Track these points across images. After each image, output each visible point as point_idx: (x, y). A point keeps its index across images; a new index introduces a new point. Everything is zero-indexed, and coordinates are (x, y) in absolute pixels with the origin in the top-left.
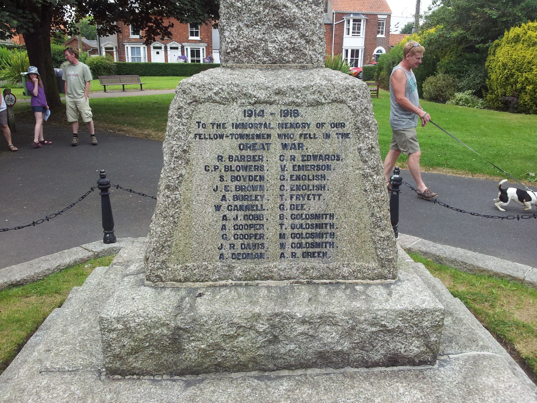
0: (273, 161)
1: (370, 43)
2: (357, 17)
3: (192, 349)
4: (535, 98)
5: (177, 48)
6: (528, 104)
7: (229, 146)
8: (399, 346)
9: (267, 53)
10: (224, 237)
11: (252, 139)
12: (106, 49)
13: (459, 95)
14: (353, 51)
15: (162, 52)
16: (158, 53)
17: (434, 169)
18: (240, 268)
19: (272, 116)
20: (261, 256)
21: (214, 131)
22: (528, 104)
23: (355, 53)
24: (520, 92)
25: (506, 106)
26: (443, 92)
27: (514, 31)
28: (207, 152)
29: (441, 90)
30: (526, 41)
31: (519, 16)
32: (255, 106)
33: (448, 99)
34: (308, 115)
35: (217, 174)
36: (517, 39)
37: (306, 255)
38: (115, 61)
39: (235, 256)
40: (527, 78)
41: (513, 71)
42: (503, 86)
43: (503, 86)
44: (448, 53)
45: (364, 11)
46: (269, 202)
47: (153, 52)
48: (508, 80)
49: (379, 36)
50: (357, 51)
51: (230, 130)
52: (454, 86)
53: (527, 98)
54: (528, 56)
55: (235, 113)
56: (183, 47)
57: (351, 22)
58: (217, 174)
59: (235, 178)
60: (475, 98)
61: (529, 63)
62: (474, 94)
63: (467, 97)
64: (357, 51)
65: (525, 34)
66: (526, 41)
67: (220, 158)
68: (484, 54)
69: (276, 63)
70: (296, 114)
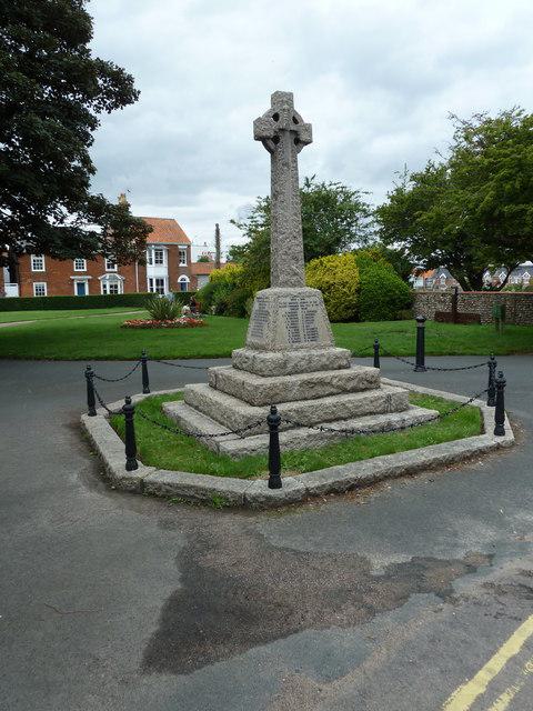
1: (174, 271)
3: (290, 367)
7: (288, 309)
11: (294, 307)
14: (157, 281)
19: (298, 300)
28: (282, 311)
34: (307, 299)
38: (87, 294)
46: (300, 325)
55: (288, 300)
57: (153, 252)
64: (162, 281)
69: (294, 285)
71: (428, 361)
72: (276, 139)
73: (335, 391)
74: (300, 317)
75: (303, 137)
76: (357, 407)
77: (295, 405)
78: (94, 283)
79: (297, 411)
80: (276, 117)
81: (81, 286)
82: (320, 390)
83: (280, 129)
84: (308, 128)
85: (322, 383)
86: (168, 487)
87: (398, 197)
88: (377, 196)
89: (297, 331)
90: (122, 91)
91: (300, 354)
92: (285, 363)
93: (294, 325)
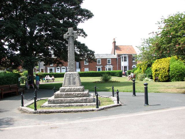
0: (71, 78)
2: (125, 56)
3: (66, 90)
5: (64, 68)
7: (68, 77)
8: (80, 90)
11: (70, 77)
12: (41, 69)
14: (125, 67)
15: (59, 70)
16: (58, 70)
23: (125, 67)
32: (70, 74)
45: (127, 54)
47: (57, 70)
49: (133, 61)
50: (126, 67)
56: (66, 68)
64: (126, 67)
71: (136, 94)
73: (74, 96)
77: (60, 99)
78: (103, 68)
79: (61, 100)
81: (99, 69)
89: (70, 82)
90: (88, 15)
91: (69, 87)
93: (70, 81)
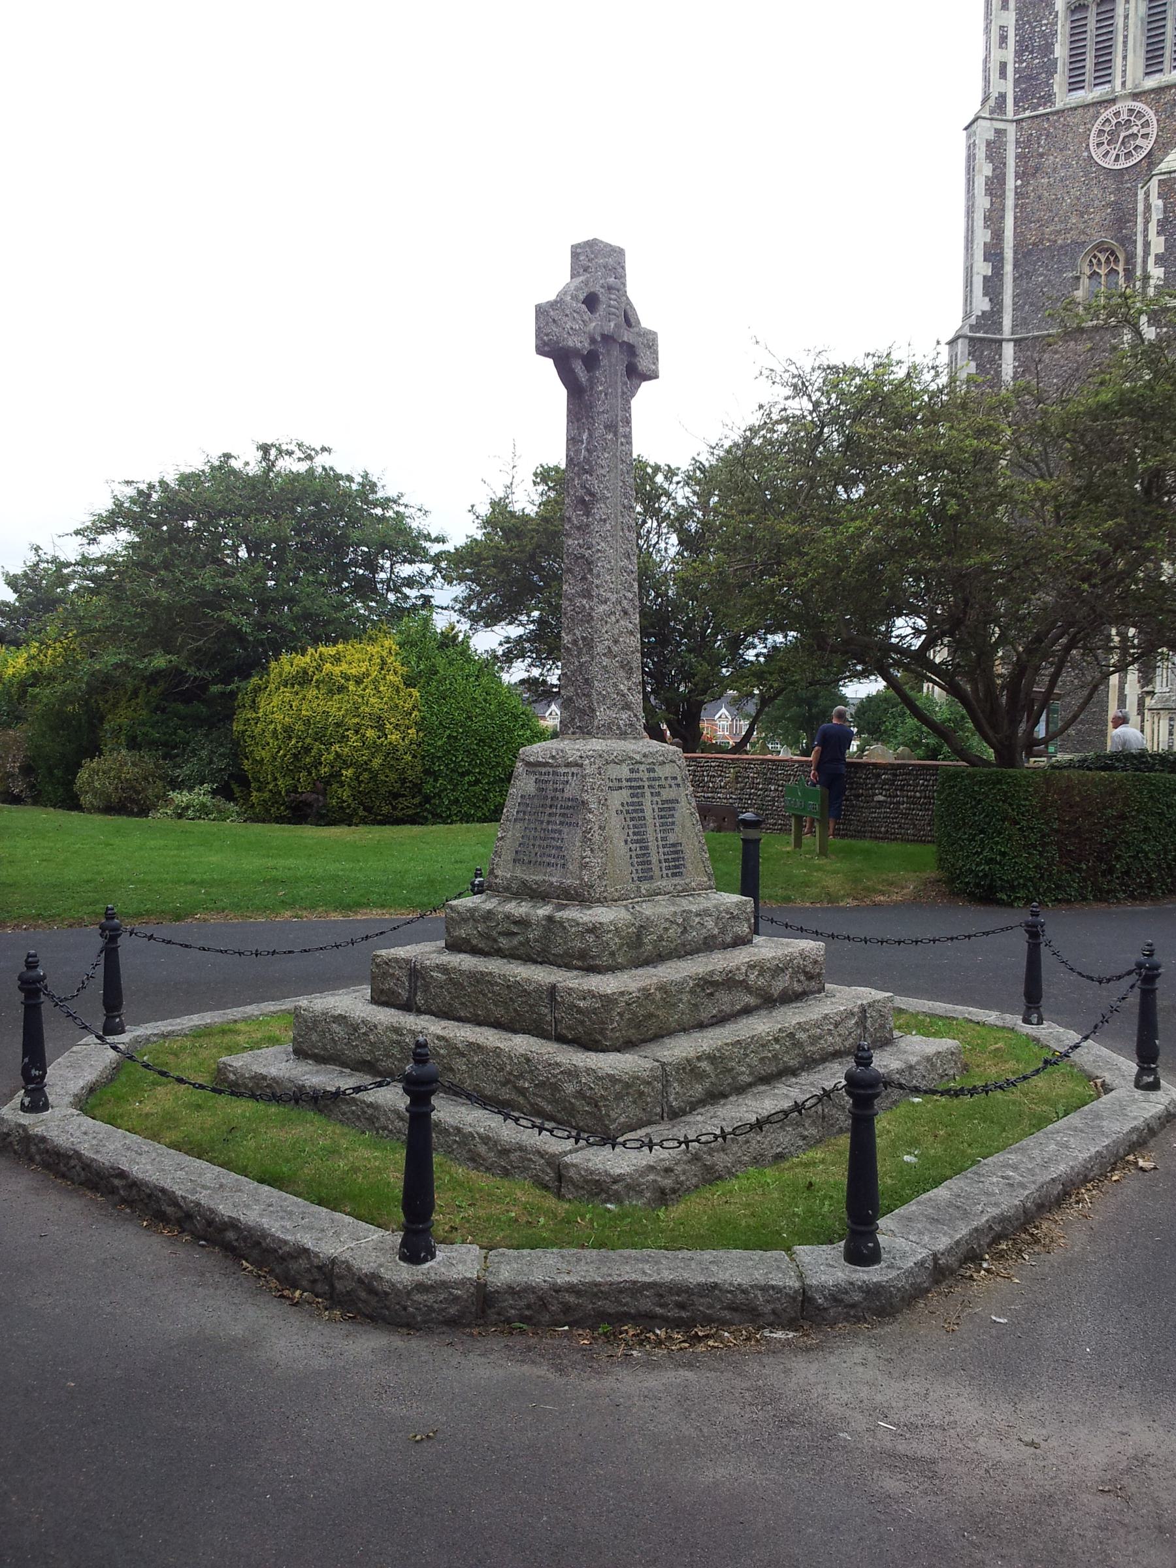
4: (360, 792)
6: (349, 806)
9: (619, 728)
10: (632, 865)
13: (181, 798)
17: (356, 913)
18: (645, 887)
20: (652, 878)
21: (617, 784)
22: (349, 806)
24: (328, 783)
25: (299, 812)
26: (138, 793)
27: (289, 663)
29: (133, 788)
30: (323, 682)
31: (292, 632)
33: (154, 807)
35: (622, 817)
36: (303, 679)
37: (674, 875)
39: (640, 879)
40: (338, 755)
41: (308, 740)
42: (288, 772)
43: (288, 772)
44: (123, 703)
48: (299, 760)
51: (625, 784)
52: (161, 778)
53: (346, 794)
54: (333, 711)
58: (622, 817)
59: (632, 819)
60: (220, 801)
61: (338, 725)
62: (214, 793)
63: (206, 799)
65: (319, 668)
66: (323, 682)
67: (622, 804)
68: (226, 708)
70: (654, 771)
72: (591, 360)
73: (751, 1000)
74: (648, 814)
75: (643, 364)
76: (814, 1040)
80: (591, 302)
82: (726, 1001)
83: (604, 336)
84: (650, 341)
85: (730, 982)
86: (571, 1299)
87: (501, 518)
88: (453, 522)
92: (639, 936)
